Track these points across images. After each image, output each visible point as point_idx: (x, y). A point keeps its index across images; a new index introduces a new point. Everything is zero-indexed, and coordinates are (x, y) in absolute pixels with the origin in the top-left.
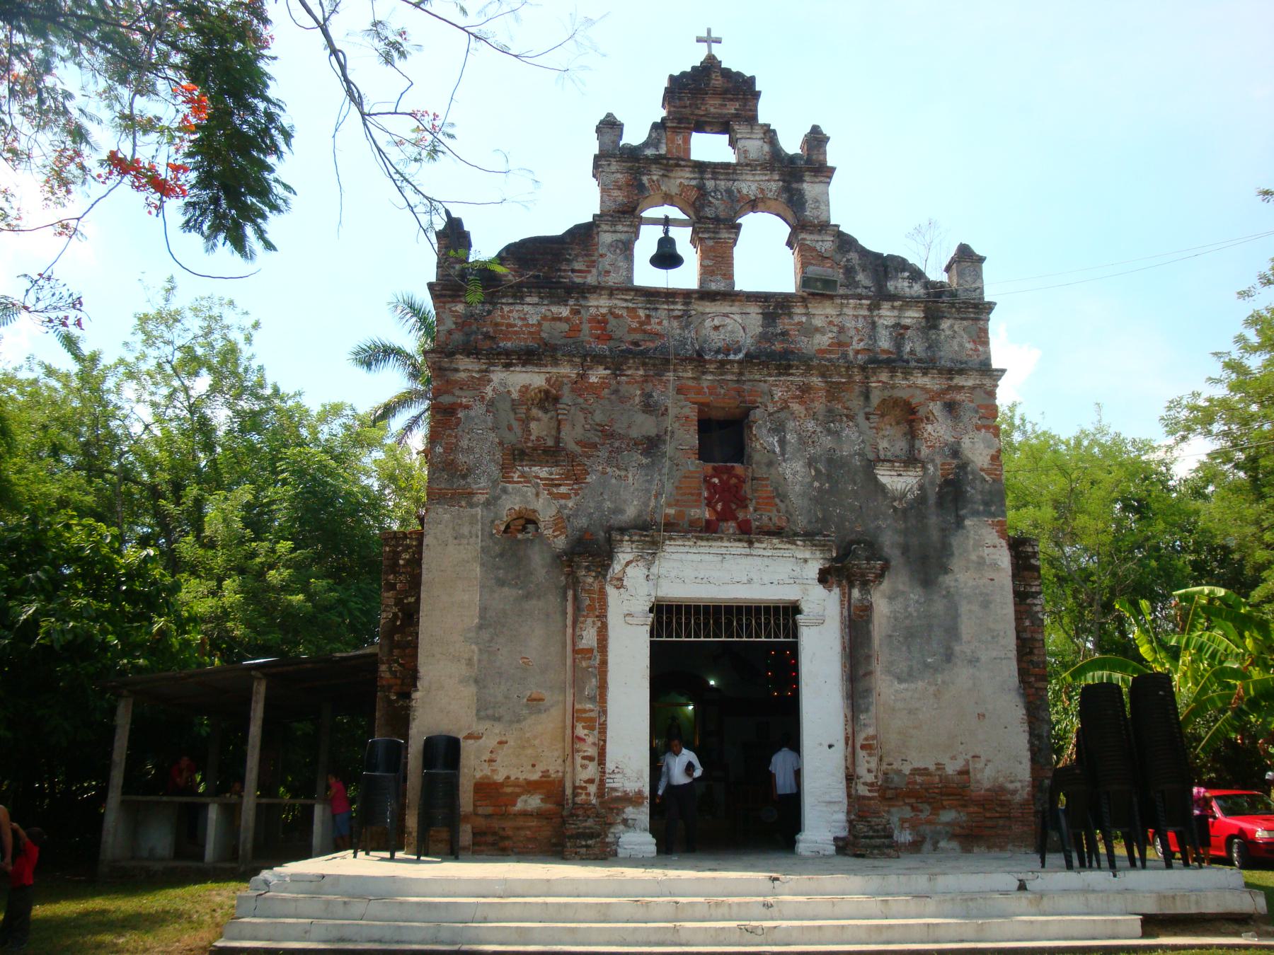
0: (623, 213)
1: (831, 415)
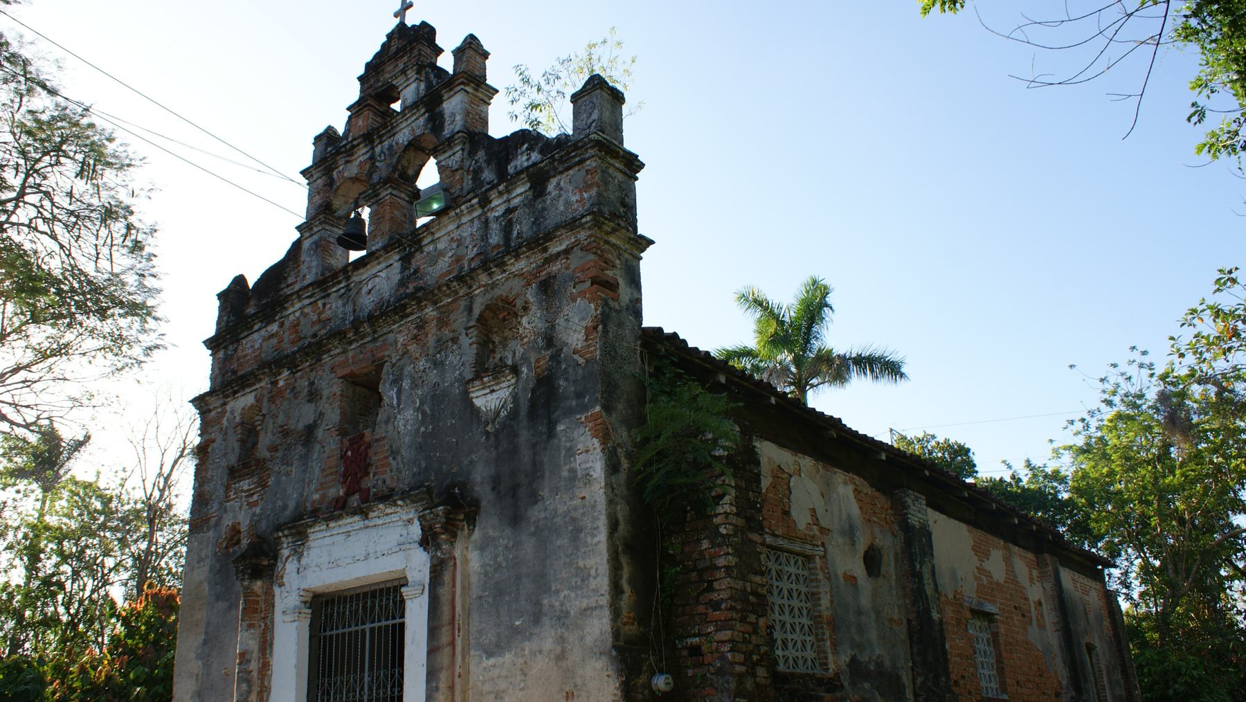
1: (441, 345)
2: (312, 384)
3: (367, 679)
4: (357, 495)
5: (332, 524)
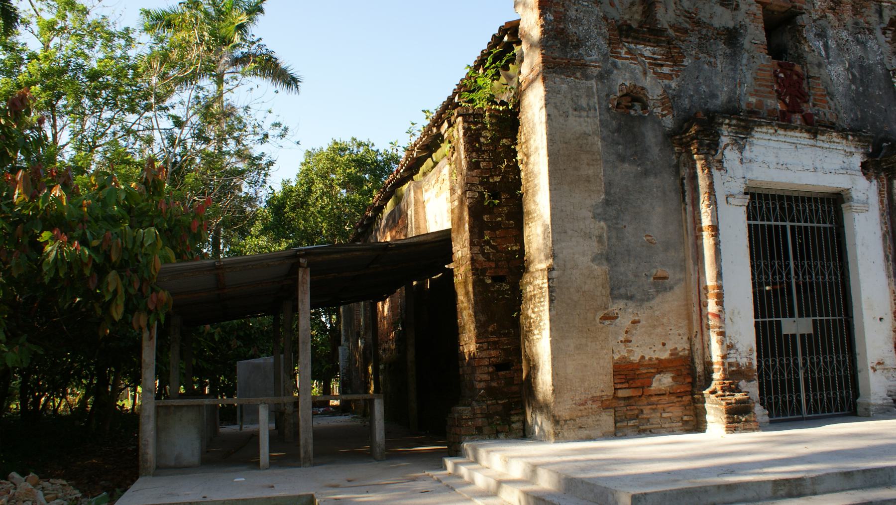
4: (796, 108)
5: (781, 132)
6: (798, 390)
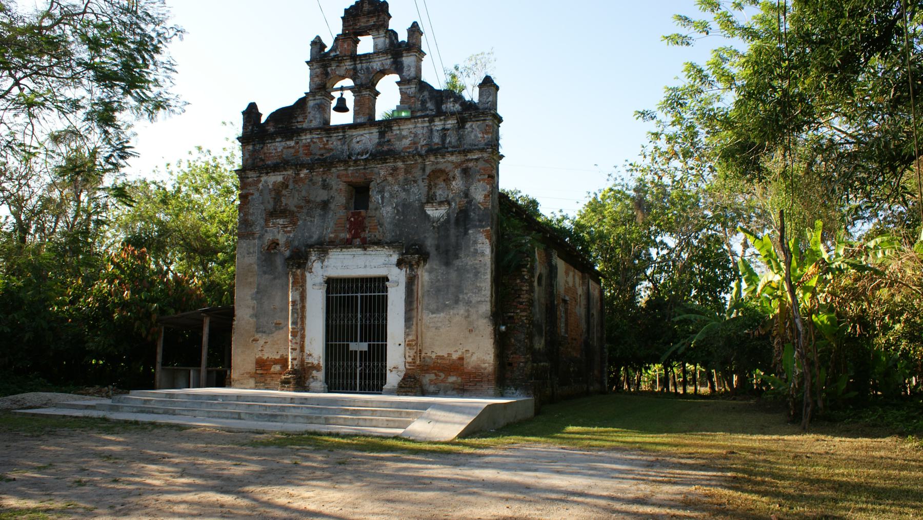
0: (321, 88)
1: (406, 181)
2: (324, 181)
3: (359, 316)
4: (358, 236)
6: (356, 378)
